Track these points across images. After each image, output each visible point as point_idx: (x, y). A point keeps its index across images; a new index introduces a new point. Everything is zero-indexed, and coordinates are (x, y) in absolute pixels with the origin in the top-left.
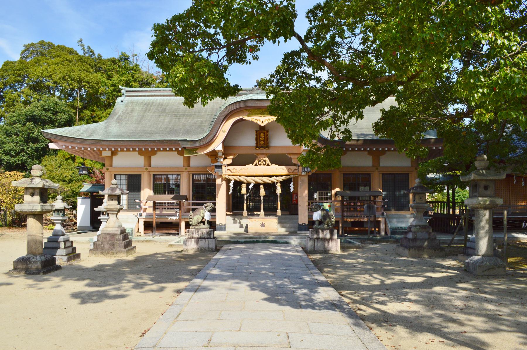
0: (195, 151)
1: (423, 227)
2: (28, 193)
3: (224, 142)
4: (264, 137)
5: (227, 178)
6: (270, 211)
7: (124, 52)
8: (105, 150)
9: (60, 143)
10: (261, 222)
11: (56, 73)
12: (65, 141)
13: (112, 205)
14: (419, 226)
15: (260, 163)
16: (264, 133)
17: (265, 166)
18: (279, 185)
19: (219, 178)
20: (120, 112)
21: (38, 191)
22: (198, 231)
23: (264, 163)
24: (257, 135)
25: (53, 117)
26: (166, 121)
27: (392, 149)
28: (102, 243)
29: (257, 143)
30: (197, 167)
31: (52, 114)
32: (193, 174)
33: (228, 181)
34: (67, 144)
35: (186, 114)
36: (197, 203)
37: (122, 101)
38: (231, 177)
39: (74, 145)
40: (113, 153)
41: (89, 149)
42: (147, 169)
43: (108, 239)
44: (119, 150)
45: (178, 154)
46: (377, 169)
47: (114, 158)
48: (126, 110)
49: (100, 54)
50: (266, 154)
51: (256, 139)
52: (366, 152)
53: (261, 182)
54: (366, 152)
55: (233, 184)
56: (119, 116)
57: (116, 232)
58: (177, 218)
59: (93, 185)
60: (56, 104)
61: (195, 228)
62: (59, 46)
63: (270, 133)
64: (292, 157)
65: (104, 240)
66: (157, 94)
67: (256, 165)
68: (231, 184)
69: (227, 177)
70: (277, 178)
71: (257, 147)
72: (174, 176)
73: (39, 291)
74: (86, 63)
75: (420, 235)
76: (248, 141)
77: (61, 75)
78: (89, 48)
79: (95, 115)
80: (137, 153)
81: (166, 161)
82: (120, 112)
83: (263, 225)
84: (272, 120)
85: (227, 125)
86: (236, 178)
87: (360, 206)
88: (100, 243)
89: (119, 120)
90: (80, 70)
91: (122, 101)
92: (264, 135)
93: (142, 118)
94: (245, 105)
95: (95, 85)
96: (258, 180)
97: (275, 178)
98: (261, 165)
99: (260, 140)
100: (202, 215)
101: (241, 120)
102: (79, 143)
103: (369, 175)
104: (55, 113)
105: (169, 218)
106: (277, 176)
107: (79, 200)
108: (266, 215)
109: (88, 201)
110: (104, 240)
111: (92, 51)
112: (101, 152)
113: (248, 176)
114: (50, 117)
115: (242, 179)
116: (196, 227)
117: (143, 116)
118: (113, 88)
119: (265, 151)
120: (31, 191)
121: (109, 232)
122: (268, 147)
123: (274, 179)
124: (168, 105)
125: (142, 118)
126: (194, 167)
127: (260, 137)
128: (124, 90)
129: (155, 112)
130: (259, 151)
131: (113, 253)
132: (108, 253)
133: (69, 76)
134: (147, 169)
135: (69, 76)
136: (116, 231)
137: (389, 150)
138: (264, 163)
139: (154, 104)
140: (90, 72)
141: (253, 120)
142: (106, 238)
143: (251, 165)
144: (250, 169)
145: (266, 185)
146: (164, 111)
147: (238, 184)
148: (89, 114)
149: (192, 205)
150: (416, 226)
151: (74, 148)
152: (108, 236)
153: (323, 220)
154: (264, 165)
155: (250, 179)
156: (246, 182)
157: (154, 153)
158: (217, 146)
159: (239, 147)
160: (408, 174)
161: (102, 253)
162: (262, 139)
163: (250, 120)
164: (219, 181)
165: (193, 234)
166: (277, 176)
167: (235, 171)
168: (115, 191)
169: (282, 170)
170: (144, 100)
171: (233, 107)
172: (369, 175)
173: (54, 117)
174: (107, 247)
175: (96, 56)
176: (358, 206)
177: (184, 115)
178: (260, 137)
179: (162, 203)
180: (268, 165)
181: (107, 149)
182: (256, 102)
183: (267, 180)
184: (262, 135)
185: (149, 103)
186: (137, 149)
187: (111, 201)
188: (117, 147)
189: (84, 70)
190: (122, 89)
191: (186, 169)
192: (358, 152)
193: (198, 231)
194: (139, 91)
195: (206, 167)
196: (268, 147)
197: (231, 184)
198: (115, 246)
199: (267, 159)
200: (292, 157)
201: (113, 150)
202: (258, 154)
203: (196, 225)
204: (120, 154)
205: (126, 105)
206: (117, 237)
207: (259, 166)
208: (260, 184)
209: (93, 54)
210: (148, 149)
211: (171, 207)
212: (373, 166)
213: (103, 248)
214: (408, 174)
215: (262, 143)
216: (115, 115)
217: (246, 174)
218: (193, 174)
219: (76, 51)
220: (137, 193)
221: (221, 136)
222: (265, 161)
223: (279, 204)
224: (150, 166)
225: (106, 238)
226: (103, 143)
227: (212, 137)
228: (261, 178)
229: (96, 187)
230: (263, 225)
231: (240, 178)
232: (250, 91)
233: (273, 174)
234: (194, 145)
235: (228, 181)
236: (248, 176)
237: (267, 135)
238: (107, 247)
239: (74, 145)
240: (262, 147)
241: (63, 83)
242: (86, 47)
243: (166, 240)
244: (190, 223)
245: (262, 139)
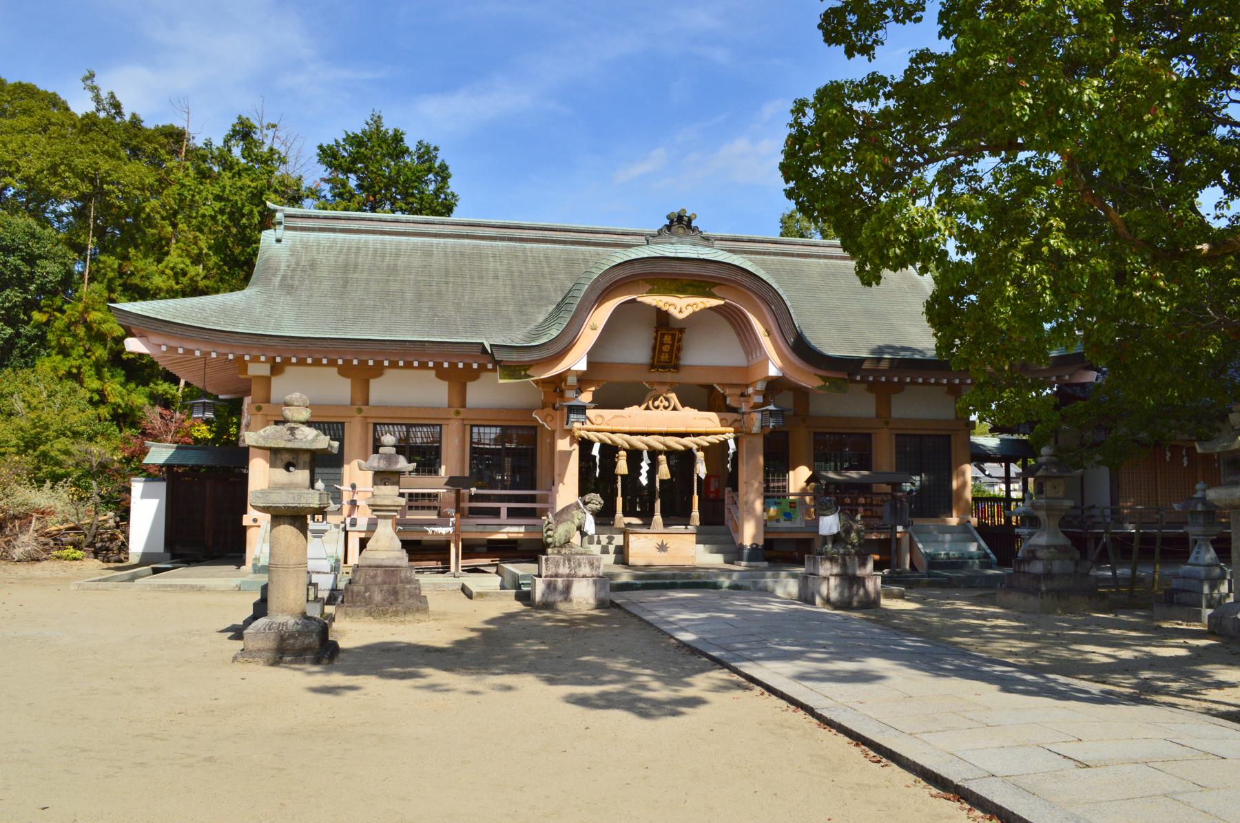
0: (525, 370)
1: (1061, 549)
2: (278, 462)
3: (590, 354)
4: (672, 345)
5: (583, 438)
6: (676, 514)
7: (244, 117)
8: (255, 359)
9: (155, 339)
10: (657, 540)
11: (26, 154)
12: (170, 335)
13: (385, 497)
14: (1055, 547)
15: (657, 403)
16: (673, 336)
17: (669, 412)
18: (700, 455)
19: (563, 437)
20: (283, 266)
21: (307, 458)
22: (569, 560)
23: (666, 404)
24: (656, 339)
25: (26, 269)
26: (409, 295)
27: (920, 380)
28: (367, 590)
29: (653, 358)
30: (485, 410)
31: (23, 259)
32: (375, 424)
33: (585, 445)
34: (173, 343)
35: (451, 279)
36: (500, 495)
37: (279, 241)
38: (592, 436)
39: (190, 346)
40: (276, 369)
41: (214, 355)
42: (360, 411)
43: (379, 579)
44: (386, 363)
45: (437, 376)
46: (887, 423)
47: (276, 382)
48: (297, 264)
49: (137, 113)
50: (671, 384)
51: (654, 348)
52: (335, 370)
53: (661, 447)
54: (335, 370)
55: (600, 452)
56: (284, 277)
57: (398, 563)
58: (451, 530)
59: (178, 448)
60: (33, 235)
61: (559, 553)
62: (20, 86)
63: (685, 336)
64: (728, 391)
65: (370, 581)
66: (363, 228)
67: (647, 408)
68: (595, 451)
69: (583, 433)
70: (697, 439)
71: (652, 366)
72: (493, 430)
73: (427, 695)
74: (106, 134)
75: (1057, 566)
76: (635, 351)
77: (46, 162)
78: (113, 96)
79: (132, 268)
80: (433, 373)
81: (402, 390)
82: (283, 266)
83: (662, 548)
84: (701, 306)
85: (601, 315)
86: (605, 437)
87: (863, 505)
88: (363, 589)
89: (287, 287)
90: (95, 152)
91: (279, 241)
92: (673, 340)
93: (345, 286)
94: (648, 268)
95: (138, 193)
96: (656, 442)
97: (692, 438)
98: (657, 408)
99: (661, 351)
100: (577, 521)
101: (634, 301)
102: (208, 342)
103: (869, 436)
104: (31, 260)
105: (430, 530)
106: (707, 434)
107: (137, 486)
108: (666, 525)
109: (162, 487)
110: (370, 581)
111: (117, 106)
112: (244, 366)
113: (631, 434)
114: (17, 269)
115: (618, 439)
116: (563, 551)
117: (346, 282)
118: (218, 205)
119: (669, 376)
120: (287, 457)
121: (379, 562)
122: (677, 367)
123: (688, 441)
124: (398, 255)
125: (345, 286)
126: (476, 409)
127: (662, 344)
128: (283, 212)
129: (370, 271)
130: (657, 376)
131: (396, 613)
132: (384, 613)
133: (69, 166)
134: (360, 411)
135: (69, 166)
136: (398, 558)
137: (914, 383)
138: (666, 404)
139: (363, 251)
140: (119, 158)
141: (661, 305)
142: (375, 576)
143: (636, 407)
144: (634, 417)
145: (670, 453)
146: (393, 269)
147: (610, 451)
148: (116, 266)
149: (470, 501)
150: (1048, 547)
151: (192, 352)
152: (379, 571)
153: (843, 535)
154: (665, 408)
155: (637, 442)
156: (627, 446)
157: (378, 370)
158: (577, 361)
159: (612, 364)
160: (949, 436)
161: (370, 614)
162: (666, 348)
163: (654, 303)
164: (563, 444)
165: (557, 566)
166: (707, 434)
167: (599, 420)
168: (397, 462)
169: (708, 421)
170: (334, 241)
171: (622, 274)
172: (869, 436)
173: (28, 269)
174: (378, 597)
175: (127, 118)
176: (859, 505)
177: (447, 283)
178: (662, 344)
179: (429, 495)
180: (675, 409)
181: (263, 359)
182: (673, 263)
183: (676, 443)
184: (667, 339)
185: (349, 249)
186: (431, 364)
187: (383, 487)
188: (289, 352)
189: (106, 152)
190: (275, 211)
191: (458, 413)
192: (419, 372)
193: (569, 560)
194: (317, 217)
195: (531, 410)
196: (677, 367)
197: (595, 451)
198: (400, 597)
199: (673, 396)
200: (728, 391)
201: (278, 360)
202: (651, 384)
203: (561, 546)
204: (390, 374)
205: (293, 251)
206: (403, 575)
207: (655, 411)
208: (660, 452)
209: (119, 113)
210: (362, 361)
211: (419, 503)
212: (878, 416)
213: (368, 601)
214: (949, 436)
215: (664, 357)
216: (274, 275)
217: (627, 428)
218: (375, 424)
219: (64, 102)
220: (337, 470)
221: (588, 338)
222: (667, 399)
223: (619, 500)
224: (366, 403)
225: (375, 576)
226: (271, 343)
227: (567, 340)
228: (661, 438)
229: (183, 452)
230: (662, 548)
231: (614, 437)
232: (649, 239)
233: (690, 429)
234: (526, 357)
235: (585, 445)
236: (631, 434)
237: (680, 340)
238: (378, 597)
239: (190, 346)
240: (664, 367)
241: (53, 184)
242: (104, 94)
243: (435, 584)
244: (549, 540)
245: (666, 348)
